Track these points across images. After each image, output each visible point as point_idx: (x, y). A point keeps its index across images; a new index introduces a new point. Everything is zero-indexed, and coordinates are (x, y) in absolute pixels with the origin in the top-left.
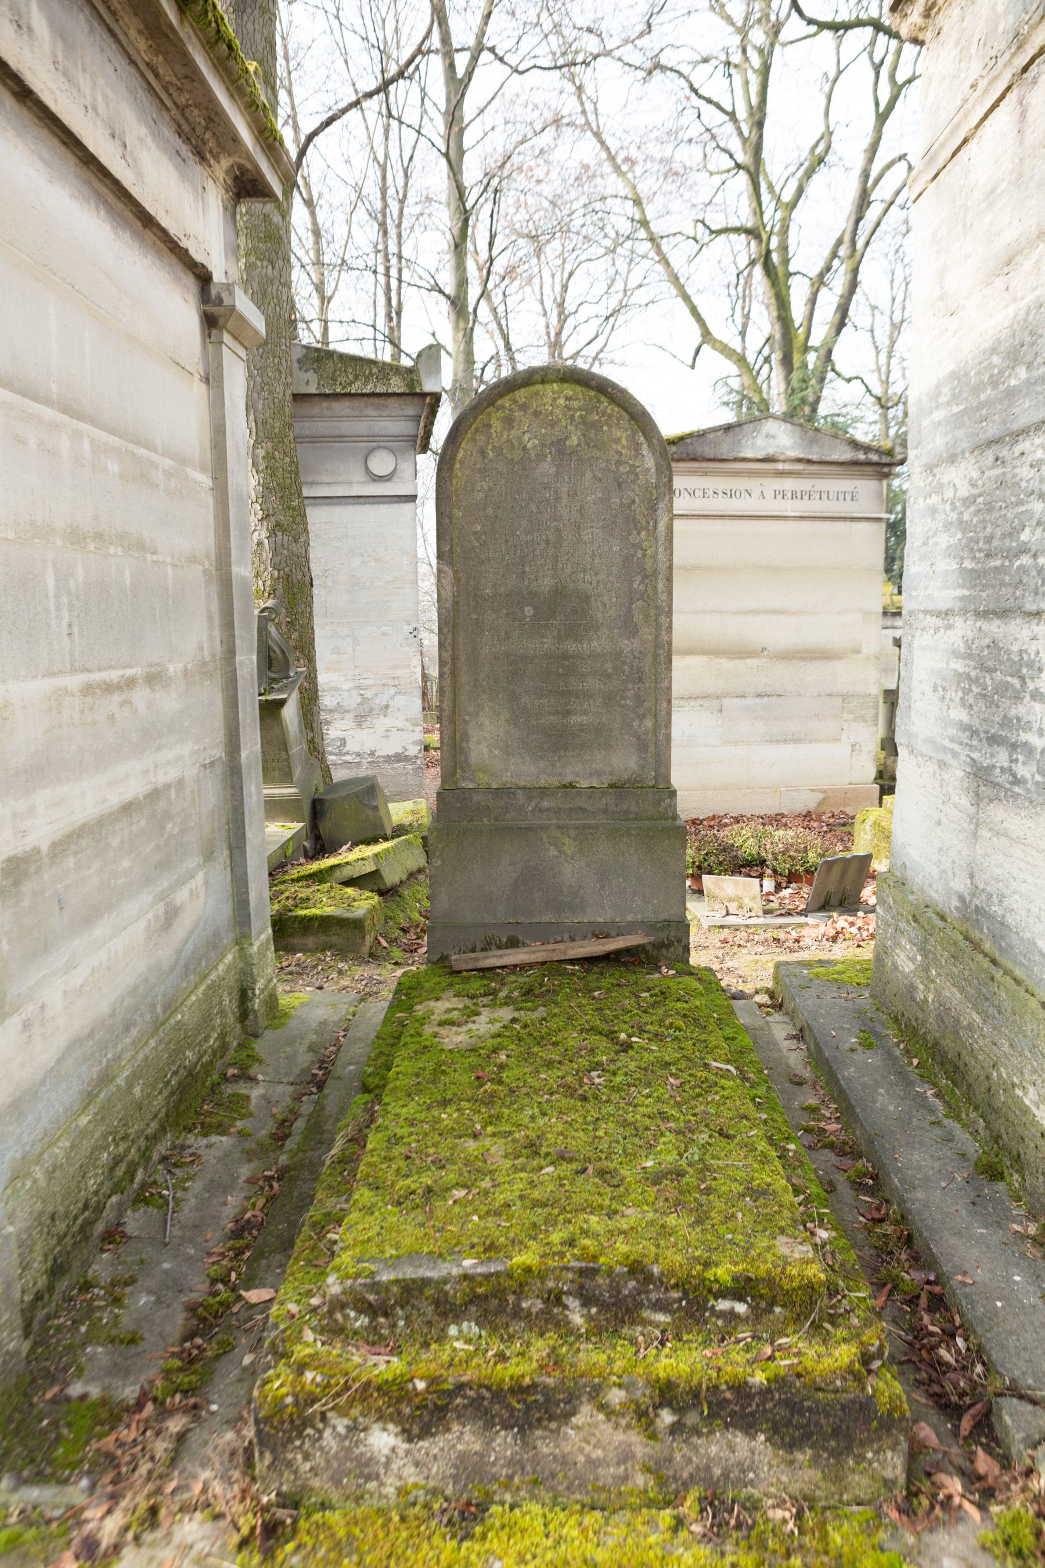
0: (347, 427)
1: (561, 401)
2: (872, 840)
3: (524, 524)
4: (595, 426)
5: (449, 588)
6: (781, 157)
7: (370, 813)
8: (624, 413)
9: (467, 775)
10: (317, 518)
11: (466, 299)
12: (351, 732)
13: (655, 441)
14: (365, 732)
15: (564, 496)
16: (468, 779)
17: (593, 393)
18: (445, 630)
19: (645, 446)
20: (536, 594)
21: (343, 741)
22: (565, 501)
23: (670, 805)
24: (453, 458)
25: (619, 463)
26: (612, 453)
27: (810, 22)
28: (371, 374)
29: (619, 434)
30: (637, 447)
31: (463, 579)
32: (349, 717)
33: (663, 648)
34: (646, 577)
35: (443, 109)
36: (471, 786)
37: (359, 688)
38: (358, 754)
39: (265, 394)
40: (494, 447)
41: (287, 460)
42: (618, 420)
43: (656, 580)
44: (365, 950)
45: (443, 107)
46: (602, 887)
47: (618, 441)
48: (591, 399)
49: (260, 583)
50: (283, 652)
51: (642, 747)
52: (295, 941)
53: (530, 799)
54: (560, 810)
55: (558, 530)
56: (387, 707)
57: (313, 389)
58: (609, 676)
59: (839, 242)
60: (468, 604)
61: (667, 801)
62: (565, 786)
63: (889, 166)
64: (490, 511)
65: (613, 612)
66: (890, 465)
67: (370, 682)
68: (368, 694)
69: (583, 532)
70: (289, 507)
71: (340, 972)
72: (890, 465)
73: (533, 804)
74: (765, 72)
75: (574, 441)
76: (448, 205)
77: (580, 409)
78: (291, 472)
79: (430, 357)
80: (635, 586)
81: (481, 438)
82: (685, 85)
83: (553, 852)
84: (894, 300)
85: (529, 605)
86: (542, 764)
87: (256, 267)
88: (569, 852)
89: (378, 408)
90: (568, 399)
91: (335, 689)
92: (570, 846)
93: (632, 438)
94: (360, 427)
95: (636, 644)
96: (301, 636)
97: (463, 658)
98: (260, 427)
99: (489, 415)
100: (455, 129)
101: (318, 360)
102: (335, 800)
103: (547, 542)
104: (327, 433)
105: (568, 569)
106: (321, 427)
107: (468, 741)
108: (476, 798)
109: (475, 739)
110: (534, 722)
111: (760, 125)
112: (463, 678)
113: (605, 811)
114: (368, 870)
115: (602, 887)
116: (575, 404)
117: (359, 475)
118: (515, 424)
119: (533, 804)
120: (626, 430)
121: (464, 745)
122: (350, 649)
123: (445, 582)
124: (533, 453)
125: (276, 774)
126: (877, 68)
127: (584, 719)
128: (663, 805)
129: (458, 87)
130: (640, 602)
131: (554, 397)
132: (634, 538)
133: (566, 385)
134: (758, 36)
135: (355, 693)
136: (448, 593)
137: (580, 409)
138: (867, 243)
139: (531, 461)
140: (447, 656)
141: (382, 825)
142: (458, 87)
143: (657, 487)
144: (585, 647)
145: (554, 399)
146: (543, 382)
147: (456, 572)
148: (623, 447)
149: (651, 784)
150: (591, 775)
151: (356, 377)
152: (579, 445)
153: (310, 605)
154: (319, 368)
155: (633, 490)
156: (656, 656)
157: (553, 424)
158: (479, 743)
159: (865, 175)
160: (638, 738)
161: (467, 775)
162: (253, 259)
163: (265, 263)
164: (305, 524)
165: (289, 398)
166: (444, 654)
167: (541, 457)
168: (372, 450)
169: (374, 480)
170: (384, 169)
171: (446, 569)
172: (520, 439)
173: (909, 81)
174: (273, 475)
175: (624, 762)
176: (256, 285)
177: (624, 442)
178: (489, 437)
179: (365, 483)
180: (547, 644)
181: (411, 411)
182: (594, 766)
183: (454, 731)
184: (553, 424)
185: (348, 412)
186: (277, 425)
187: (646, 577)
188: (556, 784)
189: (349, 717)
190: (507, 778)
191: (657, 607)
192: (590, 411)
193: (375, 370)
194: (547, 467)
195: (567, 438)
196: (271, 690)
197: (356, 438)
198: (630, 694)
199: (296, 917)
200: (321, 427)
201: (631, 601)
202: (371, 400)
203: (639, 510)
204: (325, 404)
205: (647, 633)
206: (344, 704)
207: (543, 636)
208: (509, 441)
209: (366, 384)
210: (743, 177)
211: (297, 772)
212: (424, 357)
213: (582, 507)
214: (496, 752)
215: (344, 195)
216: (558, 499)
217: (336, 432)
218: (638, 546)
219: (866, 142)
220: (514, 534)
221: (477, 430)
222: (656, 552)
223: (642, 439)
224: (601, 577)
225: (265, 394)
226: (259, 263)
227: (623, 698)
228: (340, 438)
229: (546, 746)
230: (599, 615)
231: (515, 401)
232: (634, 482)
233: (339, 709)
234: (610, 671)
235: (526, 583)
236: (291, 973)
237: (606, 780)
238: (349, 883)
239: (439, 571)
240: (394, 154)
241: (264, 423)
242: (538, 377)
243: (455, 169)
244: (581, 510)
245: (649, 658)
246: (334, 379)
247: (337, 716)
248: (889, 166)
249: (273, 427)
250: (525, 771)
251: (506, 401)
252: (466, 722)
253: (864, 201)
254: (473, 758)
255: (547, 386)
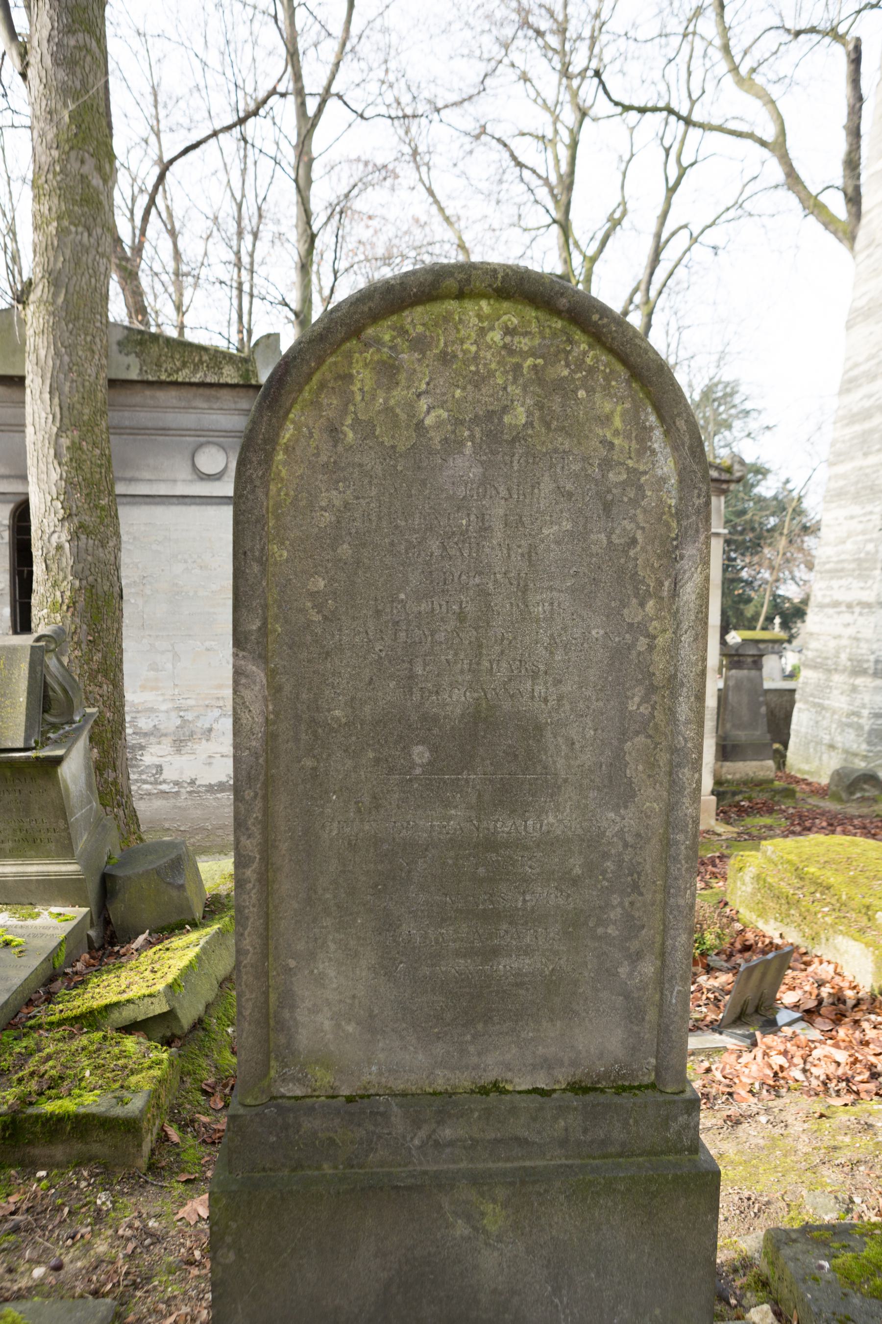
0: (172, 419)
1: (496, 336)
2: (754, 894)
3: (415, 578)
4: (561, 387)
5: (256, 708)
6: (586, 221)
7: (174, 893)
8: (619, 367)
9: (292, 1071)
10: (131, 520)
11: (310, 314)
12: (169, 758)
13: (681, 424)
14: (184, 758)
15: (498, 526)
16: (295, 1079)
17: (559, 324)
18: (248, 794)
19: (658, 433)
20: (435, 719)
21: (160, 769)
22: (498, 535)
23: (686, 1127)
24: (272, 441)
25: (607, 464)
26: (595, 443)
27: (617, 104)
28: (201, 362)
29: (608, 407)
30: (643, 433)
31: (288, 688)
32: (167, 742)
33: (684, 830)
34: (652, 689)
35: (294, 142)
36: (299, 1092)
37: (179, 709)
38: (176, 783)
39: (74, 376)
40: (356, 420)
41: (97, 452)
42: (607, 379)
43: (674, 696)
44: (142, 1163)
45: (294, 141)
46: (557, 1290)
47: (606, 420)
48: (554, 335)
49: (58, 594)
50: (65, 691)
51: (634, 1013)
52: (36, 1151)
53: (417, 1123)
54: (475, 1142)
55: (483, 593)
56: (210, 730)
57: (134, 375)
58: (575, 882)
59: (636, 290)
60: (297, 740)
61: (682, 1119)
62: (484, 1091)
63: (673, 234)
64: (345, 550)
65: (587, 758)
66: (728, 482)
67: (191, 702)
68: (189, 716)
69: (533, 598)
70: (96, 507)
71: (99, 1217)
72: (728, 482)
73: (422, 1134)
74: (574, 145)
75: (519, 416)
76: (296, 226)
77: (533, 353)
78: (100, 466)
79: (267, 346)
80: (632, 707)
81: (331, 402)
82: (507, 155)
83: (461, 1229)
84: (669, 346)
85: (422, 742)
86: (439, 1049)
87: (69, 232)
88: (493, 1229)
89: (208, 399)
90: (509, 331)
91: (152, 710)
92: (494, 1218)
93: (634, 418)
94: (188, 419)
95: (629, 819)
96: (104, 657)
97: (284, 847)
98: (66, 413)
99: (349, 356)
100: (305, 159)
101: (141, 343)
102: (129, 878)
103: (461, 617)
104: (150, 424)
105: (502, 672)
106: (143, 418)
107: (293, 1007)
108: (308, 1124)
109: (308, 1004)
110: (426, 970)
111: (569, 187)
112: (285, 885)
113: (563, 1143)
114: (158, 1011)
115: (557, 1290)
116: (524, 343)
117: (185, 472)
118: (402, 377)
119: (422, 1134)
120: (622, 400)
121: (286, 1014)
122: (169, 666)
123: (248, 695)
124: (436, 438)
125: (52, 846)
126: (667, 151)
127: (526, 964)
128: (674, 1126)
129: (308, 126)
130: (641, 739)
131: (480, 326)
132: (632, 614)
133: (506, 305)
134: (569, 116)
135: (174, 714)
136: (255, 717)
137: (533, 353)
138: (660, 293)
139: (431, 452)
140: (251, 845)
141: (190, 909)
142: (308, 126)
143: (679, 515)
144: (532, 826)
145: (482, 332)
146: (460, 296)
147: (272, 674)
148: (616, 433)
149: (646, 1080)
150: (534, 1067)
151: (184, 365)
152: (529, 424)
153: (119, 620)
154: (142, 352)
155: (633, 519)
156: (667, 844)
157: (479, 381)
158: (315, 1010)
159: (658, 235)
160: (627, 996)
161: (292, 1071)
162: (66, 223)
163: (80, 229)
164: (117, 526)
165: (103, 382)
166: (245, 841)
167: (451, 445)
168: (201, 446)
169: (202, 479)
170: (240, 206)
171: (252, 668)
172: (410, 406)
173: (692, 165)
174: (79, 468)
175: (601, 1041)
176: (68, 252)
177: (618, 422)
178: (347, 400)
179: (191, 481)
180: (456, 819)
181: (244, 404)
182: (541, 1050)
183: (266, 994)
184: (479, 381)
185: (175, 402)
186: (86, 411)
187: (652, 689)
188: (468, 1085)
189: (167, 742)
190: (370, 1076)
191: (673, 750)
192: (552, 357)
193: (205, 358)
194: (465, 466)
195: (505, 409)
196: (44, 742)
197: (182, 432)
198: (615, 914)
199: (38, 1117)
200: (143, 418)
201: (623, 736)
202: (201, 390)
203: (644, 557)
204: (148, 393)
205: (651, 798)
206: (161, 727)
207: (447, 805)
208: (388, 410)
209: (195, 372)
210: (555, 228)
211: (82, 842)
212: (261, 346)
213: (532, 548)
214: (350, 1028)
215: (201, 226)
216: (485, 530)
217: (161, 424)
218: (640, 629)
219: (659, 211)
220: (394, 599)
221: (322, 385)
222: (676, 642)
223: (653, 419)
224: (566, 688)
225: (74, 376)
226: (73, 229)
227: (601, 922)
228: (164, 431)
229: (448, 1016)
230: (561, 763)
231: (402, 331)
232: (634, 503)
233: (155, 732)
234: (577, 871)
235: (416, 697)
236: (16, 1230)
237: (562, 1077)
238: (130, 1028)
239: (238, 673)
240: (250, 195)
241: (71, 408)
242: (451, 284)
243: (303, 187)
244: (530, 555)
245: (653, 848)
246: (159, 365)
247: (153, 739)
248: (673, 234)
249: (81, 414)
250: (409, 1063)
251: (384, 331)
252: (288, 970)
253: (655, 260)
254: (303, 1039)
255: (468, 305)
